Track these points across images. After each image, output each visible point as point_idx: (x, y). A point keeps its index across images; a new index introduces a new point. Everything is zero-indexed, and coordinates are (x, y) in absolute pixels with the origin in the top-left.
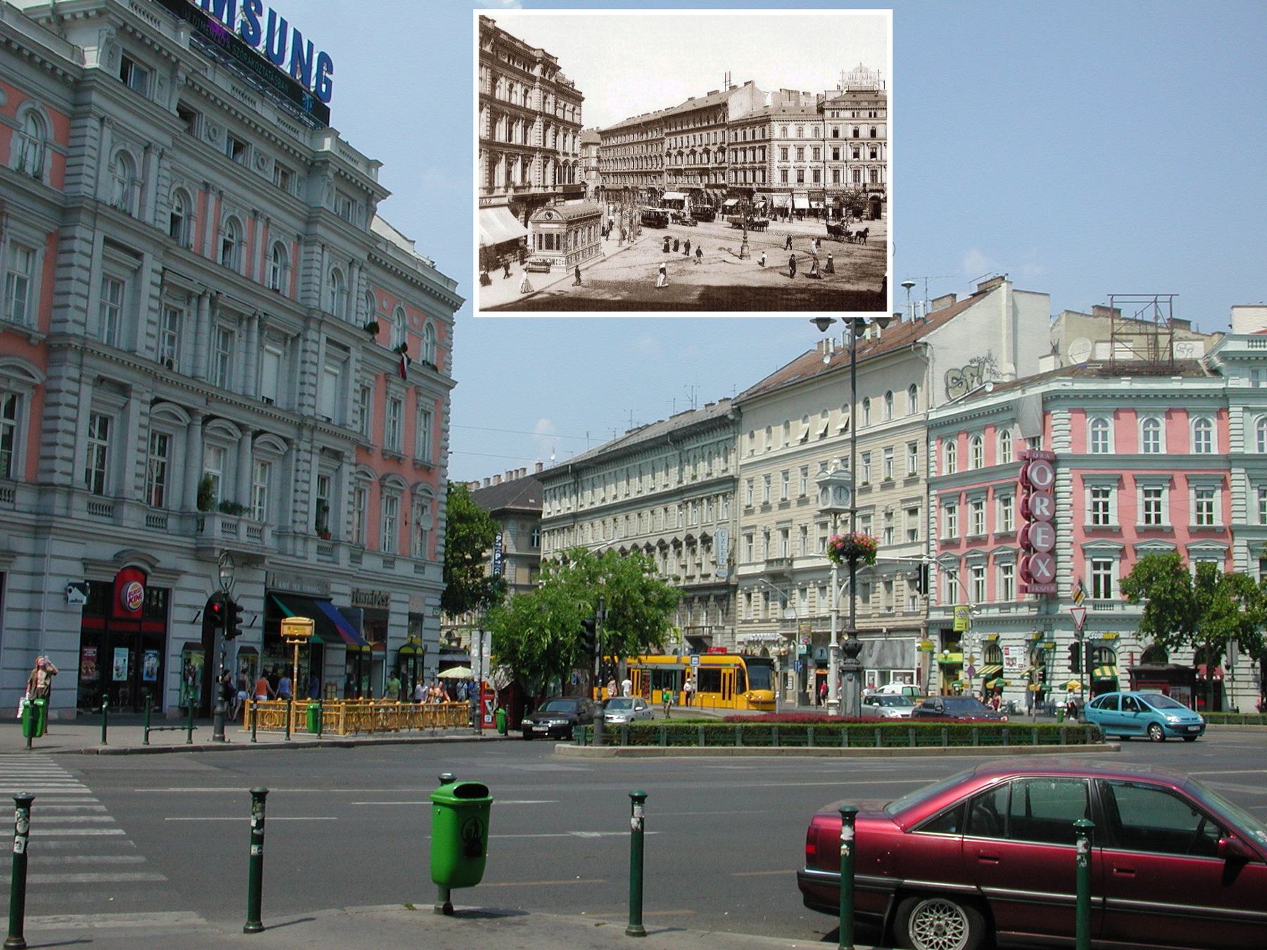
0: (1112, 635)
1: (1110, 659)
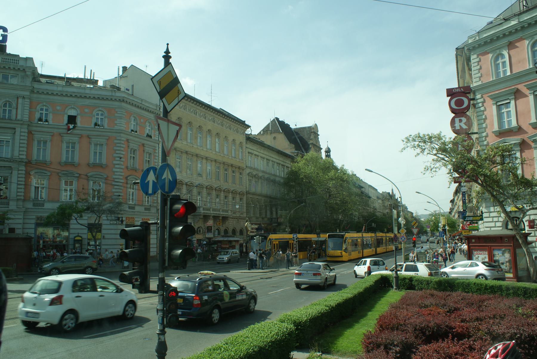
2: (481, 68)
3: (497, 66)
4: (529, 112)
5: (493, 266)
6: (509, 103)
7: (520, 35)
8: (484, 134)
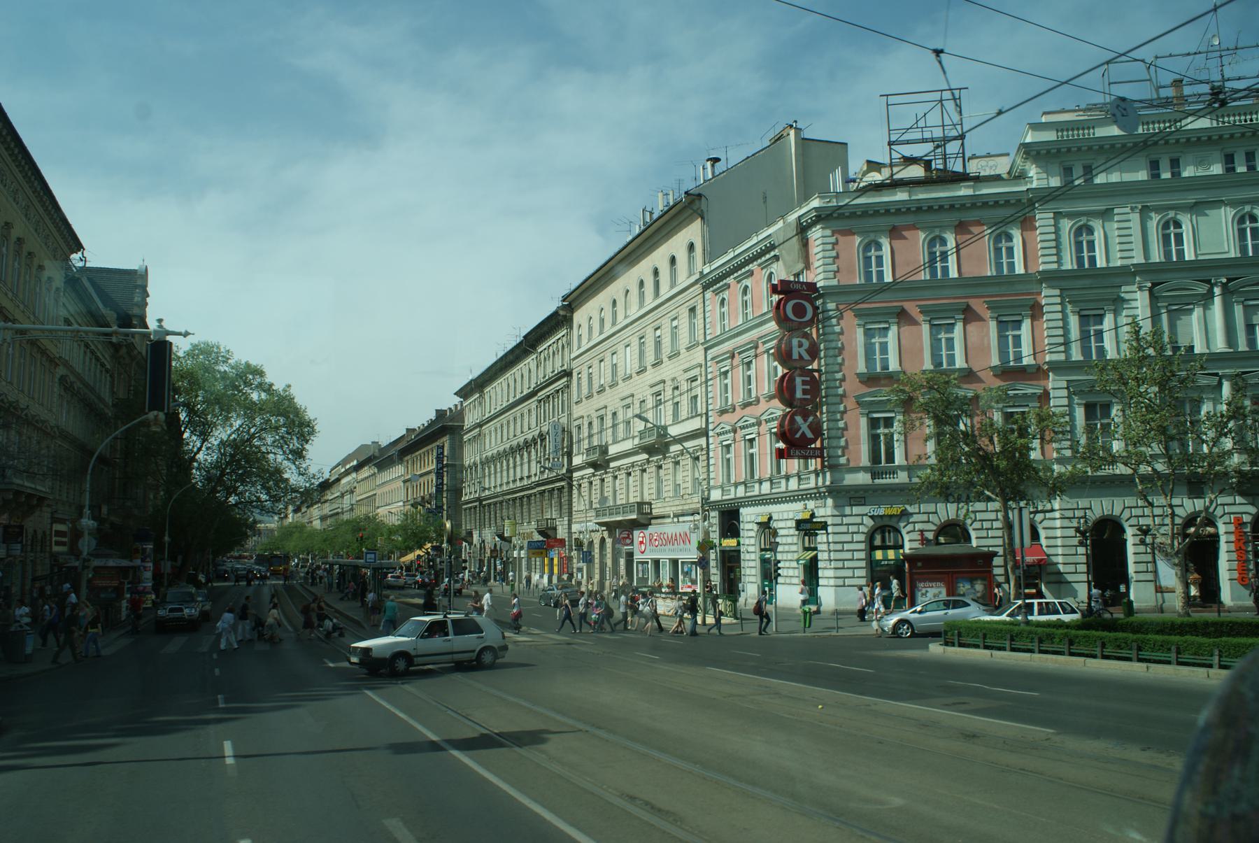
0: (896, 510)
1: (896, 541)
2: (837, 257)
3: (867, 260)
4: (921, 350)
5: (1000, 605)
6: (953, 324)
7: (910, 219)
8: (839, 376)
